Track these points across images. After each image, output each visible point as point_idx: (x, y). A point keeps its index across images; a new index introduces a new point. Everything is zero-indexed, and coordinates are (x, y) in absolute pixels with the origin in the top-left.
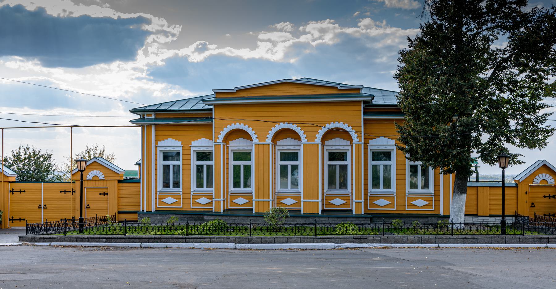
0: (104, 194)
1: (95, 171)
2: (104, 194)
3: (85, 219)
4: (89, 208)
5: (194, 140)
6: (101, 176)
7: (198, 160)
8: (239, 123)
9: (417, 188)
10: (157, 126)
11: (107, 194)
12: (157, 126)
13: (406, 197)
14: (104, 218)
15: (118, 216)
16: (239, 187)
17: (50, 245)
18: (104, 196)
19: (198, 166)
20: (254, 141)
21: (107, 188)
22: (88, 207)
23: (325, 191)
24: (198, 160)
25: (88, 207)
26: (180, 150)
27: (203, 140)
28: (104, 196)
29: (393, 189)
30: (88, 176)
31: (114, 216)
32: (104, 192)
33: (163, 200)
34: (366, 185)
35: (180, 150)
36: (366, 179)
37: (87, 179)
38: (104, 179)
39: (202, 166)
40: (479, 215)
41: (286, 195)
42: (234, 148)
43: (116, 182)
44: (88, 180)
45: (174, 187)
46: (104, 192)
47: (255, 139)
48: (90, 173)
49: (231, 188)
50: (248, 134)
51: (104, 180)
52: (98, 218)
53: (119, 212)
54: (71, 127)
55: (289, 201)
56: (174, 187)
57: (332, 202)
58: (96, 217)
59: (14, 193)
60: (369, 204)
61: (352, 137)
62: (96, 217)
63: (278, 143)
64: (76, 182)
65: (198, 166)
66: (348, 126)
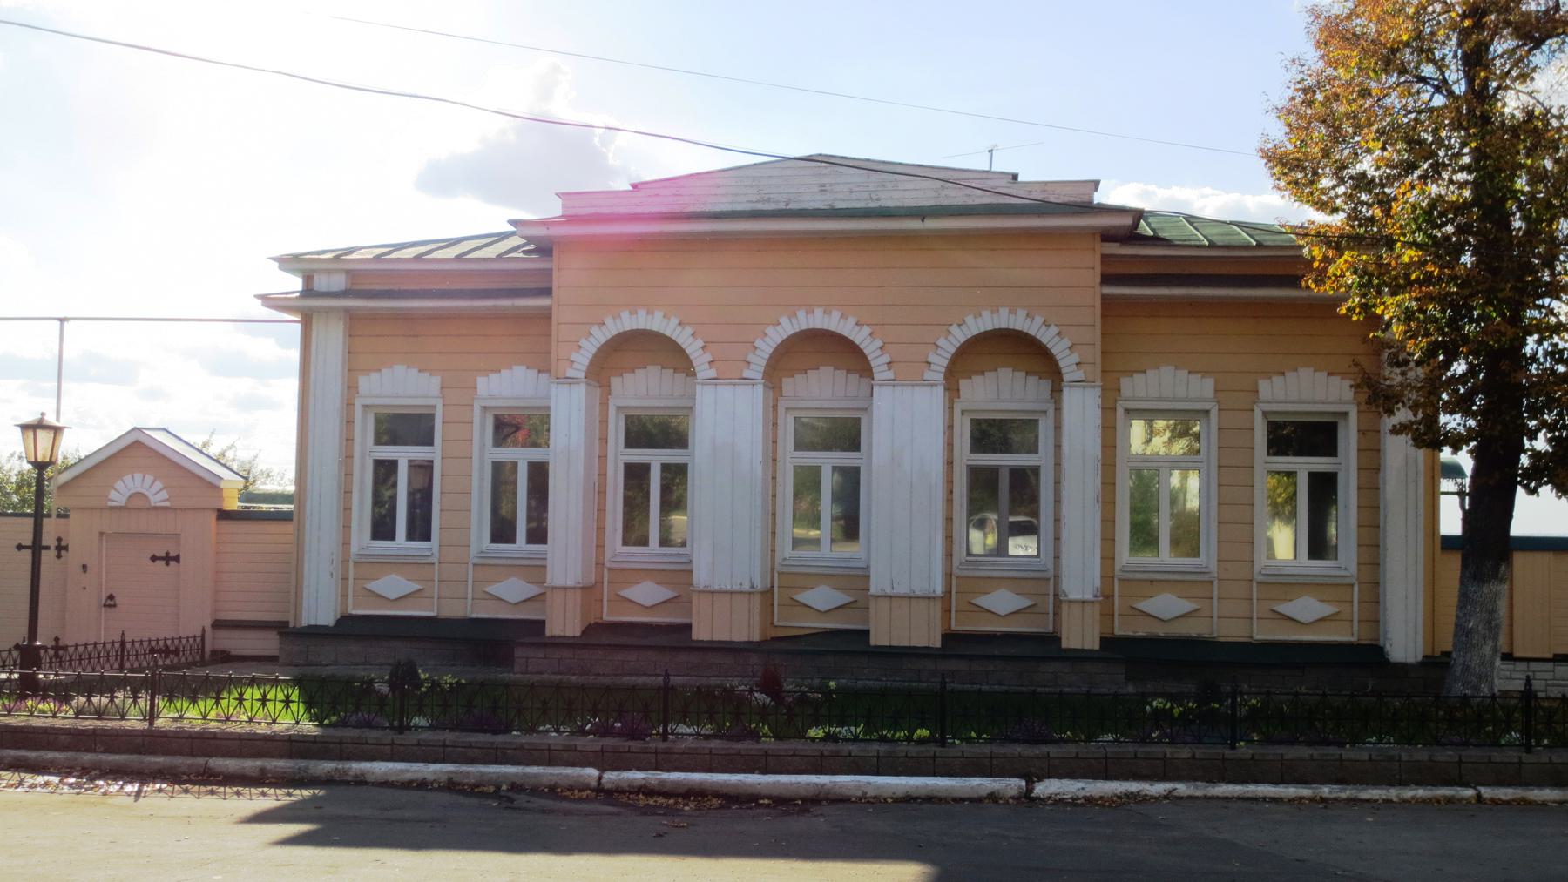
0: (168, 559)
1: (138, 476)
2: (168, 559)
3: (71, 650)
4: (115, 606)
5: (486, 372)
6: (157, 494)
7: (378, 441)
8: (1007, 310)
9: (393, 538)
10: (352, 317)
11: (177, 559)
12: (352, 317)
13: (606, 572)
14: (161, 643)
15: (214, 638)
16: (390, 535)
17: (1479, 797)
18: (167, 564)
19: (379, 464)
20: (699, 375)
21: (176, 537)
22: (109, 602)
23: (354, 549)
24: (378, 441)
25: (109, 602)
26: (434, 407)
27: (520, 372)
28: (167, 564)
29: (1208, 558)
30: (113, 495)
31: (198, 640)
32: (167, 553)
33: (373, 586)
34: (1108, 539)
35: (434, 407)
36: (1108, 521)
37: (110, 504)
38: (167, 504)
39: (817, 471)
40: (1517, 654)
41: (1156, 582)
42: (1268, 408)
43: (214, 516)
44: (112, 508)
45: (411, 536)
46: (167, 553)
47: (939, 368)
48: (119, 485)
49: (1125, 557)
50: (861, 353)
51: (166, 508)
52: (128, 646)
53: (218, 625)
54: (62, 320)
55: (822, 597)
56: (411, 536)
57: (983, 601)
58: (123, 643)
59: (28, 554)
60: (605, 598)
61: (1061, 364)
62: (123, 643)
63: (788, 384)
64: (72, 515)
65: (379, 464)
66: (1046, 324)
